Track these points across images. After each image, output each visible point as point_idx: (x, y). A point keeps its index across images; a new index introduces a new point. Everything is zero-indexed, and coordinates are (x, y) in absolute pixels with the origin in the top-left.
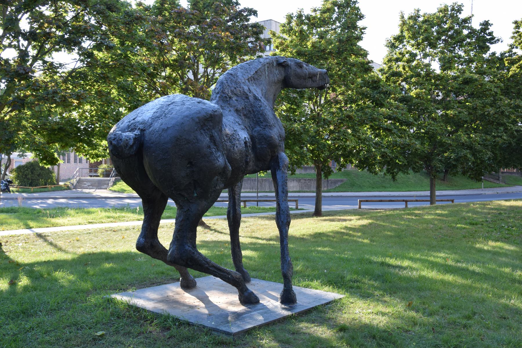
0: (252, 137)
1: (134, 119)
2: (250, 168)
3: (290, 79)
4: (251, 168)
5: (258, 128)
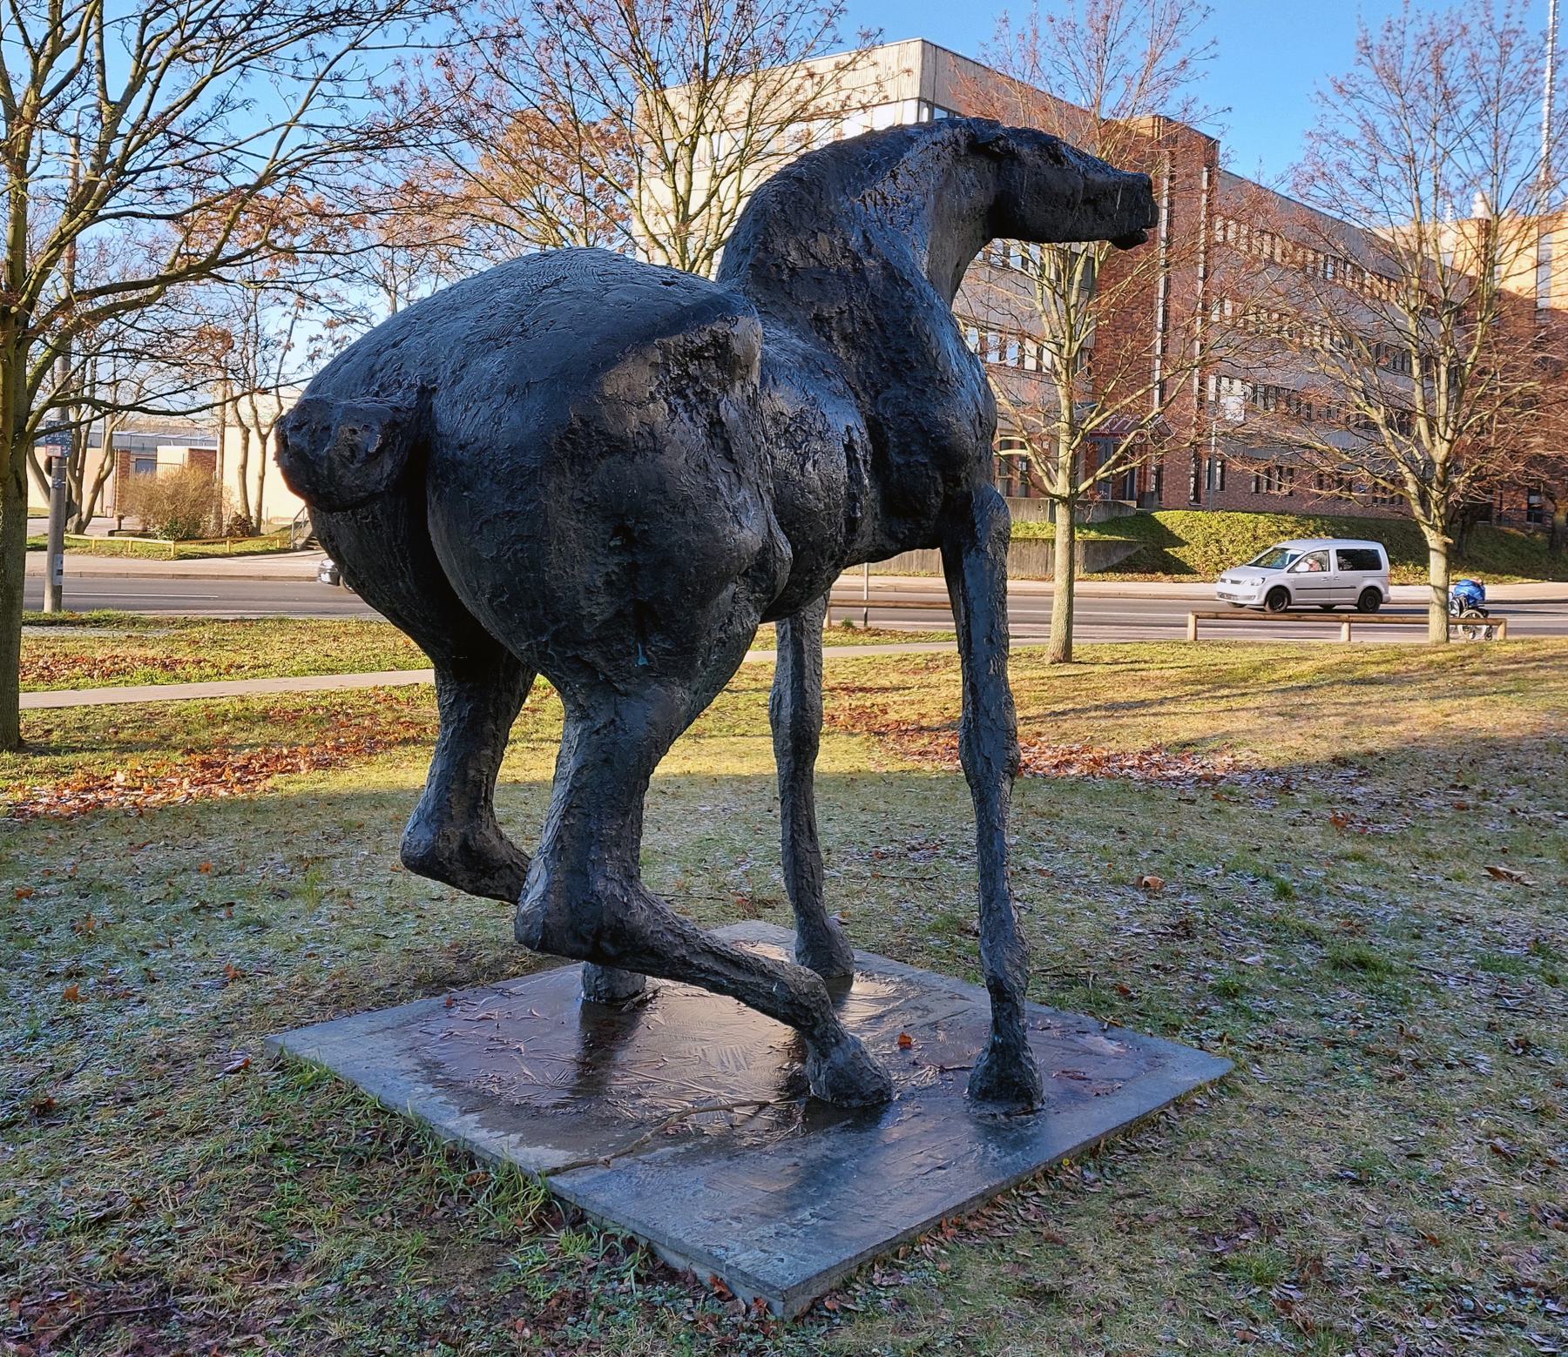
0: (875, 428)
1: (395, 345)
2: (862, 543)
3: (1018, 205)
4: (867, 540)
5: (897, 391)
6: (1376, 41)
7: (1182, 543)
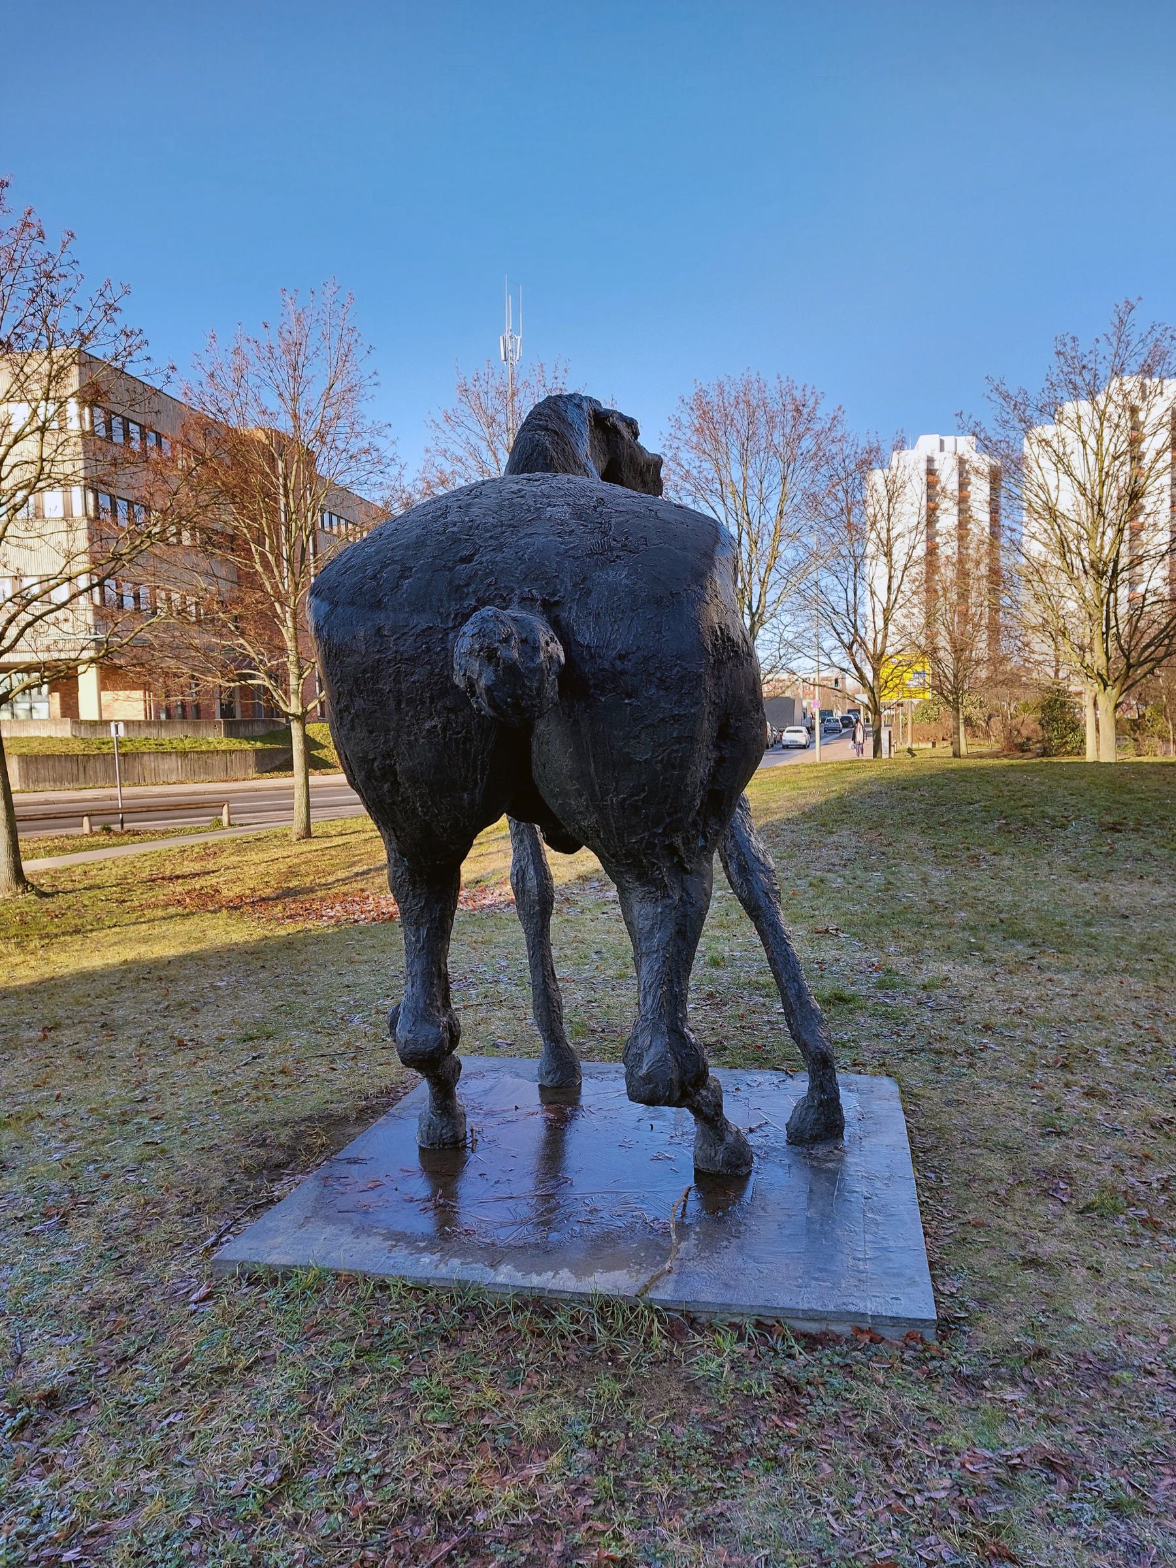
6: (470, 386)
7: (323, 747)
